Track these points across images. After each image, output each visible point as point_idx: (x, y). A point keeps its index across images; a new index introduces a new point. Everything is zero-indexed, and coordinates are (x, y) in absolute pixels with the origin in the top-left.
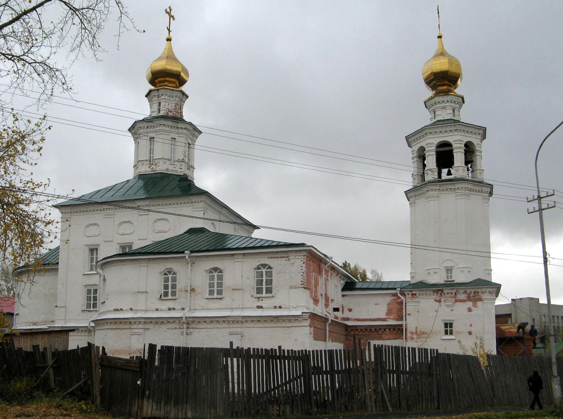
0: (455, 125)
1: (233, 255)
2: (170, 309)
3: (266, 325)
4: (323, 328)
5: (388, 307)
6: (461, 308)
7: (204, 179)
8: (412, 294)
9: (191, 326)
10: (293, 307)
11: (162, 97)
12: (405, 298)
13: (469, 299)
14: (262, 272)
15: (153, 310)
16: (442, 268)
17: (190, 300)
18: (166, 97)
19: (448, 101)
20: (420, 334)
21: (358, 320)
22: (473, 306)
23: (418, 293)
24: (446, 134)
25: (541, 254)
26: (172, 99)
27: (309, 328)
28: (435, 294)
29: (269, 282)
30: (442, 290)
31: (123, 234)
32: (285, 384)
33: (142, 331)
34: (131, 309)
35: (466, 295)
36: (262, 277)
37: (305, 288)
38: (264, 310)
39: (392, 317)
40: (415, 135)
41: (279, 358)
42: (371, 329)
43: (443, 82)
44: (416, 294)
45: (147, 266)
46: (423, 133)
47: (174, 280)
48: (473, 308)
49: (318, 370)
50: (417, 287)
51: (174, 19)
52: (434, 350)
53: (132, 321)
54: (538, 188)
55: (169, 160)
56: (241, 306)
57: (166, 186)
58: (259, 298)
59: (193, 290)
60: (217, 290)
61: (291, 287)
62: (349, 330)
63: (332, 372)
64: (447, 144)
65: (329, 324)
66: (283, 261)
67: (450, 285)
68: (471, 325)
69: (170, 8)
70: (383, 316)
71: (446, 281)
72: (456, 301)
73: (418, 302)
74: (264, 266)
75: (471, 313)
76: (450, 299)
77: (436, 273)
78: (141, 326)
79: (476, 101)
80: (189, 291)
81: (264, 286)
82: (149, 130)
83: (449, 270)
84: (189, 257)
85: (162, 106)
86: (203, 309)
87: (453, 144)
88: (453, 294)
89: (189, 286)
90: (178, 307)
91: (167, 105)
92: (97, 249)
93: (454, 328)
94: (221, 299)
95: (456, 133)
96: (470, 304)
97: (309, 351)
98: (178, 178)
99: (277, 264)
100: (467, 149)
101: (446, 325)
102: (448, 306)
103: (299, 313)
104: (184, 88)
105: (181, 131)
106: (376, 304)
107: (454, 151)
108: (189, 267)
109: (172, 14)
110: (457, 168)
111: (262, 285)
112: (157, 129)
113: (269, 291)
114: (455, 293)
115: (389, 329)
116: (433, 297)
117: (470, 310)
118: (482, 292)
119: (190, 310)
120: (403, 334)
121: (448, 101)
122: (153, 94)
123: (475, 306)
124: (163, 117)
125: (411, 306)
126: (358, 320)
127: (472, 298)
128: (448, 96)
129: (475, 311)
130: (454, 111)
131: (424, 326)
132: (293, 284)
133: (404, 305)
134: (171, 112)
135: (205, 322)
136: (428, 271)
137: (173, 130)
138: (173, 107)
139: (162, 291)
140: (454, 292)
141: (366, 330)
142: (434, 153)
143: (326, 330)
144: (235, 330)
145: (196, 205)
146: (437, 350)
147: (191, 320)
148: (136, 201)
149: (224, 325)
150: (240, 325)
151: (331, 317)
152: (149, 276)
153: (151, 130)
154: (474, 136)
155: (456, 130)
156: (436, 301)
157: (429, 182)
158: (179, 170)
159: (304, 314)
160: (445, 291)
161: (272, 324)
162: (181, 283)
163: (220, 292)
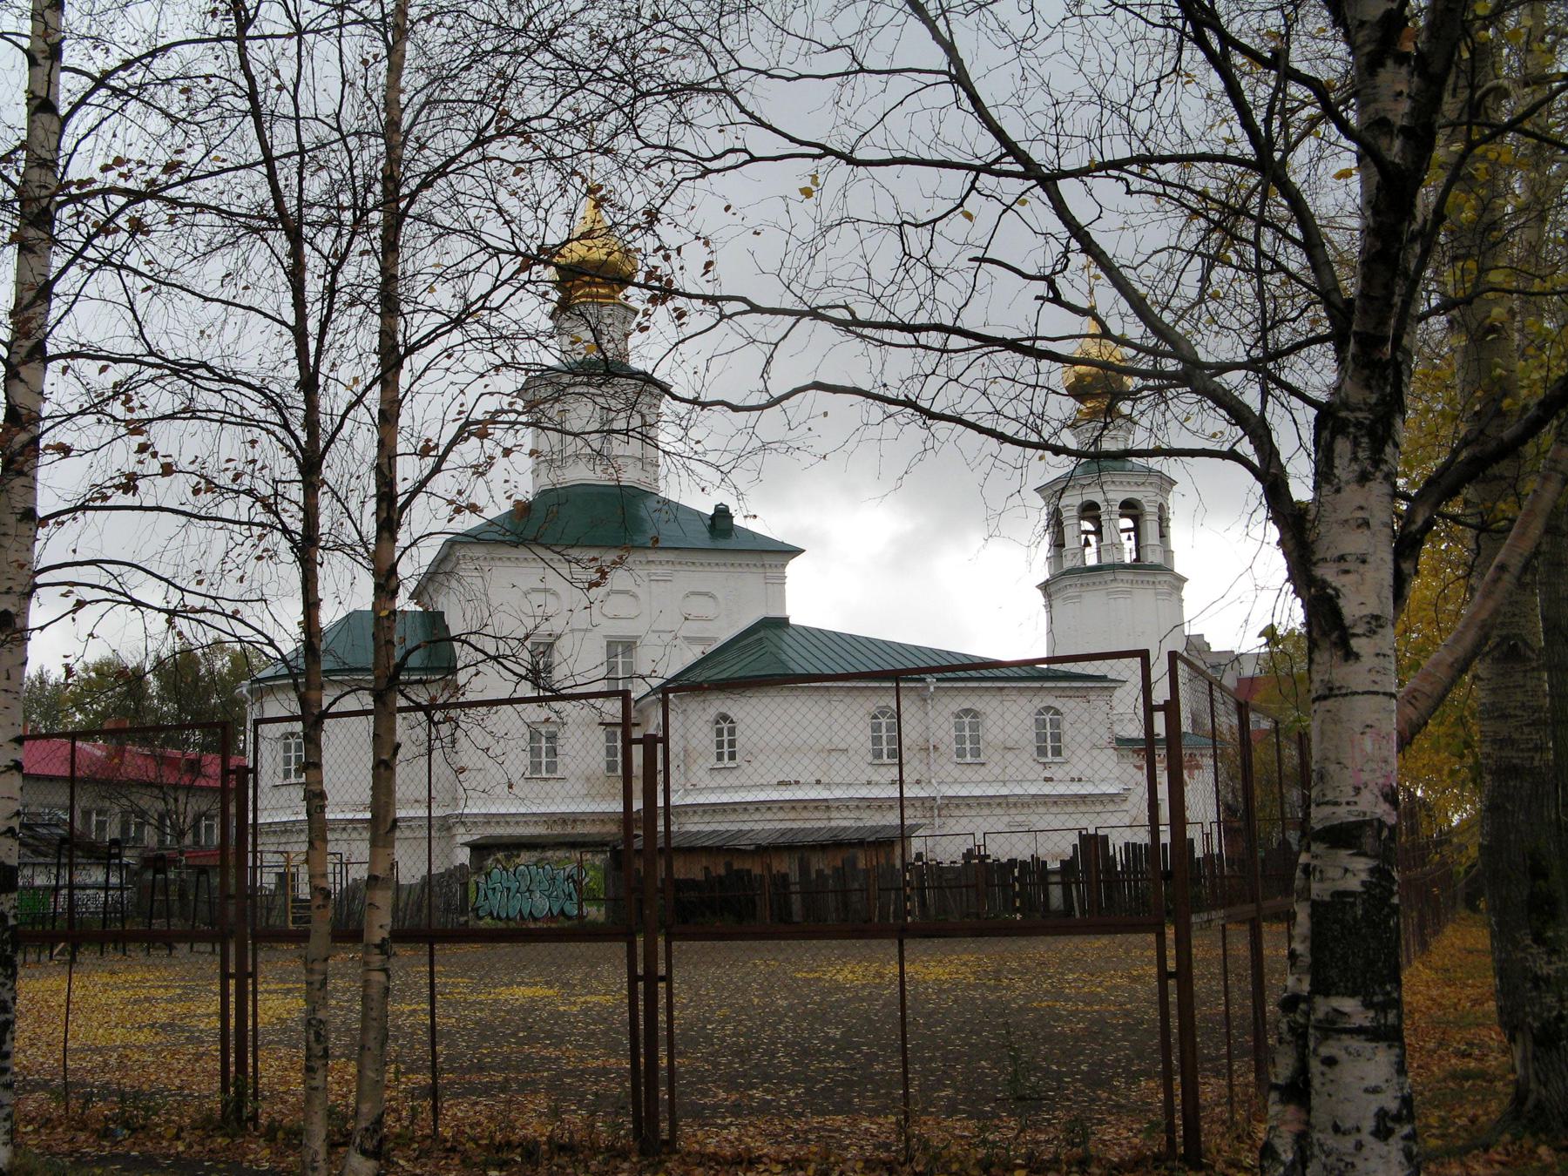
29: (1057, 738)
31: (615, 617)
53: (970, 801)
60: (970, 748)
66: (995, 703)
113: (1057, 752)
163: (976, 752)
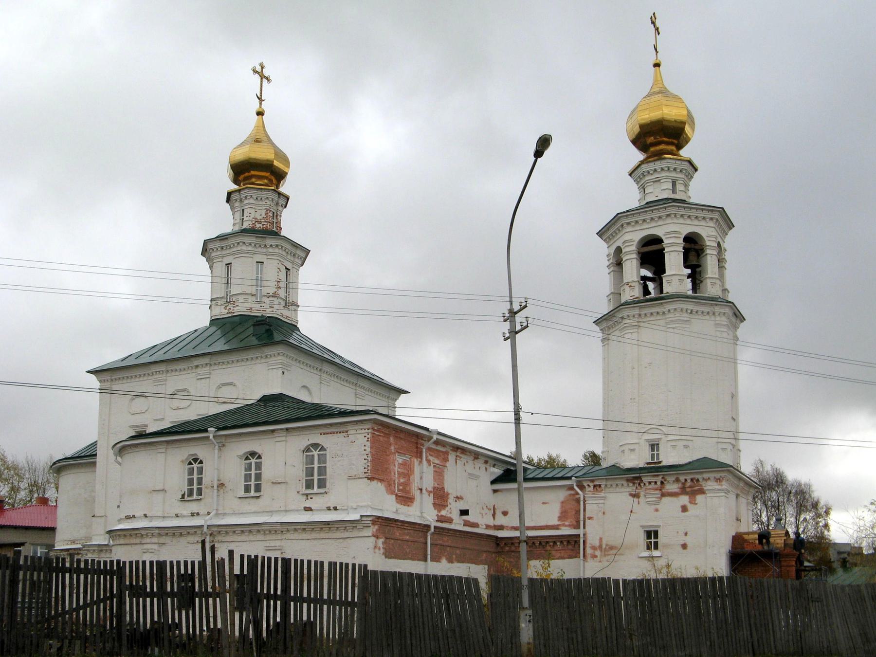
0: (665, 208)
1: (273, 431)
2: (193, 515)
3: (314, 535)
4: (422, 540)
5: (562, 507)
6: (670, 505)
7: (313, 324)
8: (595, 486)
9: (216, 539)
10: (352, 508)
11: (246, 202)
13: (683, 491)
14: (313, 456)
15: (172, 517)
16: (642, 442)
17: (218, 501)
18: (252, 201)
20: (608, 550)
22: (690, 502)
23: (603, 483)
24: (653, 224)
25: (511, 408)
26: (261, 203)
27: (373, 539)
28: (631, 484)
29: (322, 471)
30: (639, 478)
32: (77, 610)
33: (155, 547)
34: (145, 516)
35: (680, 485)
36: (313, 463)
37: (369, 479)
38: (314, 512)
39: (567, 523)
40: (608, 229)
41: (70, 571)
42: (533, 543)
43: (660, 139)
44: (600, 486)
45: (165, 453)
46: (618, 225)
47: (200, 471)
48: (689, 506)
49: (138, 591)
50: (596, 473)
52: (347, 565)
53: (143, 532)
54: (511, 297)
55: (253, 295)
56: (283, 509)
57: (260, 332)
58: (307, 495)
59: (221, 485)
60: (254, 486)
61: (350, 478)
62: (502, 545)
63: (162, 594)
64: (656, 240)
65: (433, 534)
67: (655, 468)
68: (686, 534)
70: (555, 522)
71: (648, 464)
72: (663, 495)
73: (604, 498)
74: (315, 446)
75: (687, 513)
76: (652, 492)
77: (632, 450)
78: (155, 540)
79: (713, 168)
80: (215, 487)
81: (315, 479)
82: (224, 252)
83: (654, 446)
84: (214, 437)
85: (246, 214)
86: (234, 514)
87: (663, 238)
88: (659, 483)
89: (216, 480)
90: (203, 511)
91: (255, 211)
92: (658, 444)
93: (661, 540)
94: (258, 497)
95: (669, 221)
96: (684, 499)
97: (124, 563)
98: (251, 323)
99: (332, 443)
100: (688, 246)
101: (649, 534)
102: (650, 503)
103: (356, 517)
105: (271, 250)
106: (544, 503)
107: (666, 250)
108: (216, 451)
109: (266, 73)
110: (669, 278)
111: (312, 475)
112: (235, 249)
113: (322, 484)
114: (662, 483)
115: (561, 542)
116: (628, 490)
117: (684, 509)
119: (217, 514)
121: (662, 169)
122: (234, 197)
123: (693, 502)
124: (244, 231)
125: (593, 505)
128: (663, 161)
129: (692, 510)
130: (674, 184)
131: (613, 537)
132: (353, 473)
133: (582, 503)
134: (260, 222)
135: (234, 532)
136: (622, 448)
137: (260, 250)
138: (264, 215)
139: (185, 488)
140: (659, 480)
142: (634, 256)
143: (426, 543)
144: (273, 544)
145: (271, 361)
146: (366, 566)
147: (216, 529)
148: (192, 359)
149: (260, 537)
150: (279, 537)
151: (433, 524)
152: (166, 468)
153: (228, 252)
154: (703, 223)
155: (668, 215)
157: (626, 303)
159: (364, 519)
160: (646, 480)
161: (323, 535)
162: (209, 476)
163: (258, 488)
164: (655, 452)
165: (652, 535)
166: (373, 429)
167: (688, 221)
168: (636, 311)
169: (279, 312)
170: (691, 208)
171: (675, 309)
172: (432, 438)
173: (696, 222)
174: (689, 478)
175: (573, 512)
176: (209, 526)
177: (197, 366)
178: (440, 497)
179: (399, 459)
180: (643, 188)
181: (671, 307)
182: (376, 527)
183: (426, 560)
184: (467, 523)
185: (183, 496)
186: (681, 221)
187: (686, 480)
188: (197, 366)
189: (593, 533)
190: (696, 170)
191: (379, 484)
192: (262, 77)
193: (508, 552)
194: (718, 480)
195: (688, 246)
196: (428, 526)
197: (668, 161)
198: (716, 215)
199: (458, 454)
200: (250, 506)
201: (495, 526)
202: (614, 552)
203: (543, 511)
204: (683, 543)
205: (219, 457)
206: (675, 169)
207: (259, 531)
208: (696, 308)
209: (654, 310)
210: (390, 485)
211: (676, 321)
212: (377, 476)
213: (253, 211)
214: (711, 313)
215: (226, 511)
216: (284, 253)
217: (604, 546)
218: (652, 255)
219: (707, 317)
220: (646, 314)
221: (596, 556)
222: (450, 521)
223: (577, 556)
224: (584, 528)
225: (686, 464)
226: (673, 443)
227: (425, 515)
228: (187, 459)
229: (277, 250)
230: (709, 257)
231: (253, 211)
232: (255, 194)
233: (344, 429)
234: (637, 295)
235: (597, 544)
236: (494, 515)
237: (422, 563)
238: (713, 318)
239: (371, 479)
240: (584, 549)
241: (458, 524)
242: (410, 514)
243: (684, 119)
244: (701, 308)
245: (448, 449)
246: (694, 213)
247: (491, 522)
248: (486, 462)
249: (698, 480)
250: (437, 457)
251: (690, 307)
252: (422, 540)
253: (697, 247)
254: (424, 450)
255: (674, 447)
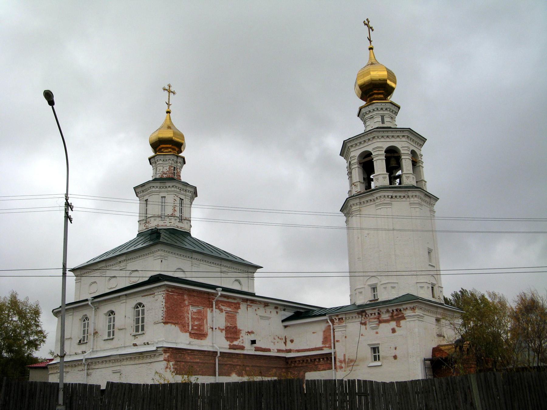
1: (119, 297)
5: (324, 334)
8: (339, 319)
12: (333, 325)
13: (392, 318)
16: (366, 287)
17: (93, 342)
18: (161, 162)
19: (374, 110)
20: (351, 363)
21: (298, 351)
22: (397, 326)
23: (344, 317)
27: (165, 362)
30: (364, 311)
35: (390, 314)
38: (138, 347)
42: (307, 360)
43: (376, 91)
44: (342, 318)
48: (397, 329)
51: (373, 30)
56: (123, 345)
67: (375, 304)
68: (396, 348)
69: (367, 19)
70: (320, 345)
71: (370, 301)
72: (380, 322)
73: (345, 326)
76: (373, 320)
82: (144, 193)
84: (91, 303)
87: (372, 152)
88: (377, 314)
91: (164, 168)
93: (381, 354)
95: (374, 141)
96: (393, 324)
100: (389, 155)
102: (373, 328)
104: (394, 98)
105: (169, 189)
106: (313, 333)
108: (93, 312)
114: (379, 314)
115: (323, 359)
116: (360, 320)
117: (394, 331)
118: (404, 309)
120: (331, 364)
121: (374, 110)
123: (398, 326)
126: (298, 351)
127: (395, 317)
128: (373, 105)
129: (399, 331)
130: (383, 118)
134: (166, 174)
137: (163, 190)
138: (168, 170)
141: (303, 361)
147: (90, 361)
150: (119, 364)
154: (398, 139)
155: (374, 138)
156: (361, 323)
158: (168, 224)
159: (158, 349)
160: (369, 312)
164: (376, 293)
165: (375, 350)
166: (168, 291)
167: (388, 140)
168: (357, 201)
169: (176, 224)
170: (392, 131)
171: (380, 197)
172: (218, 294)
173: (393, 140)
174: (394, 308)
175: (328, 338)
176: (86, 359)
177: (120, 262)
178: (232, 332)
179: (193, 309)
180: (365, 123)
181: (377, 195)
182: (168, 354)
183: (215, 376)
184: (257, 349)
185: (80, 341)
186: (383, 140)
187: (393, 311)
188: (120, 262)
189: (340, 351)
190: (399, 108)
191: (173, 326)
192: (170, 92)
193: (294, 367)
194: (413, 309)
195: (389, 155)
196: (216, 352)
197: (378, 104)
198: (406, 134)
199: (248, 303)
200: (109, 345)
201: (286, 350)
202: (352, 364)
203: (307, 339)
204: (394, 355)
205: (95, 315)
206: (382, 109)
207: (110, 361)
208: (394, 195)
209: (368, 199)
210: (184, 326)
211: (380, 204)
212: (170, 321)
213: (161, 168)
214: (406, 196)
215: (98, 349)
216: (178, 190)
217: (347, 360)
218: (367, 165)
219: (404, 199)
220: (364, 202)
221: (342, 368)
222: (242, 348)
223: (331, 368)
224: (334, 348)
225: (394, 299)
226: (385, 286)
227: (214, 345)
228: (82, 318)
229: (173, 189)
230: (403, 161)
231: (161, 168)
232: (162, 158)
233: (152, 293)
234: (359, 190)
235: (342, 359)
236: (285, 343)
237: (214, 377)
238: (408, 199)
239: (165, 323)
240: (335, 363)
241: (249, 350)
242: (204, 345)
243: (386, 77)
244: (398, 194)
245: (240, 301)
246: (396, 134)
247: (283, 347)
248: (276, 308)
249: (400, 310)
250: (229, 307)
251: (390, 194)
252: (213, 362)
253: (396, 155)
254: (214, 303)
255: (385, 288)
